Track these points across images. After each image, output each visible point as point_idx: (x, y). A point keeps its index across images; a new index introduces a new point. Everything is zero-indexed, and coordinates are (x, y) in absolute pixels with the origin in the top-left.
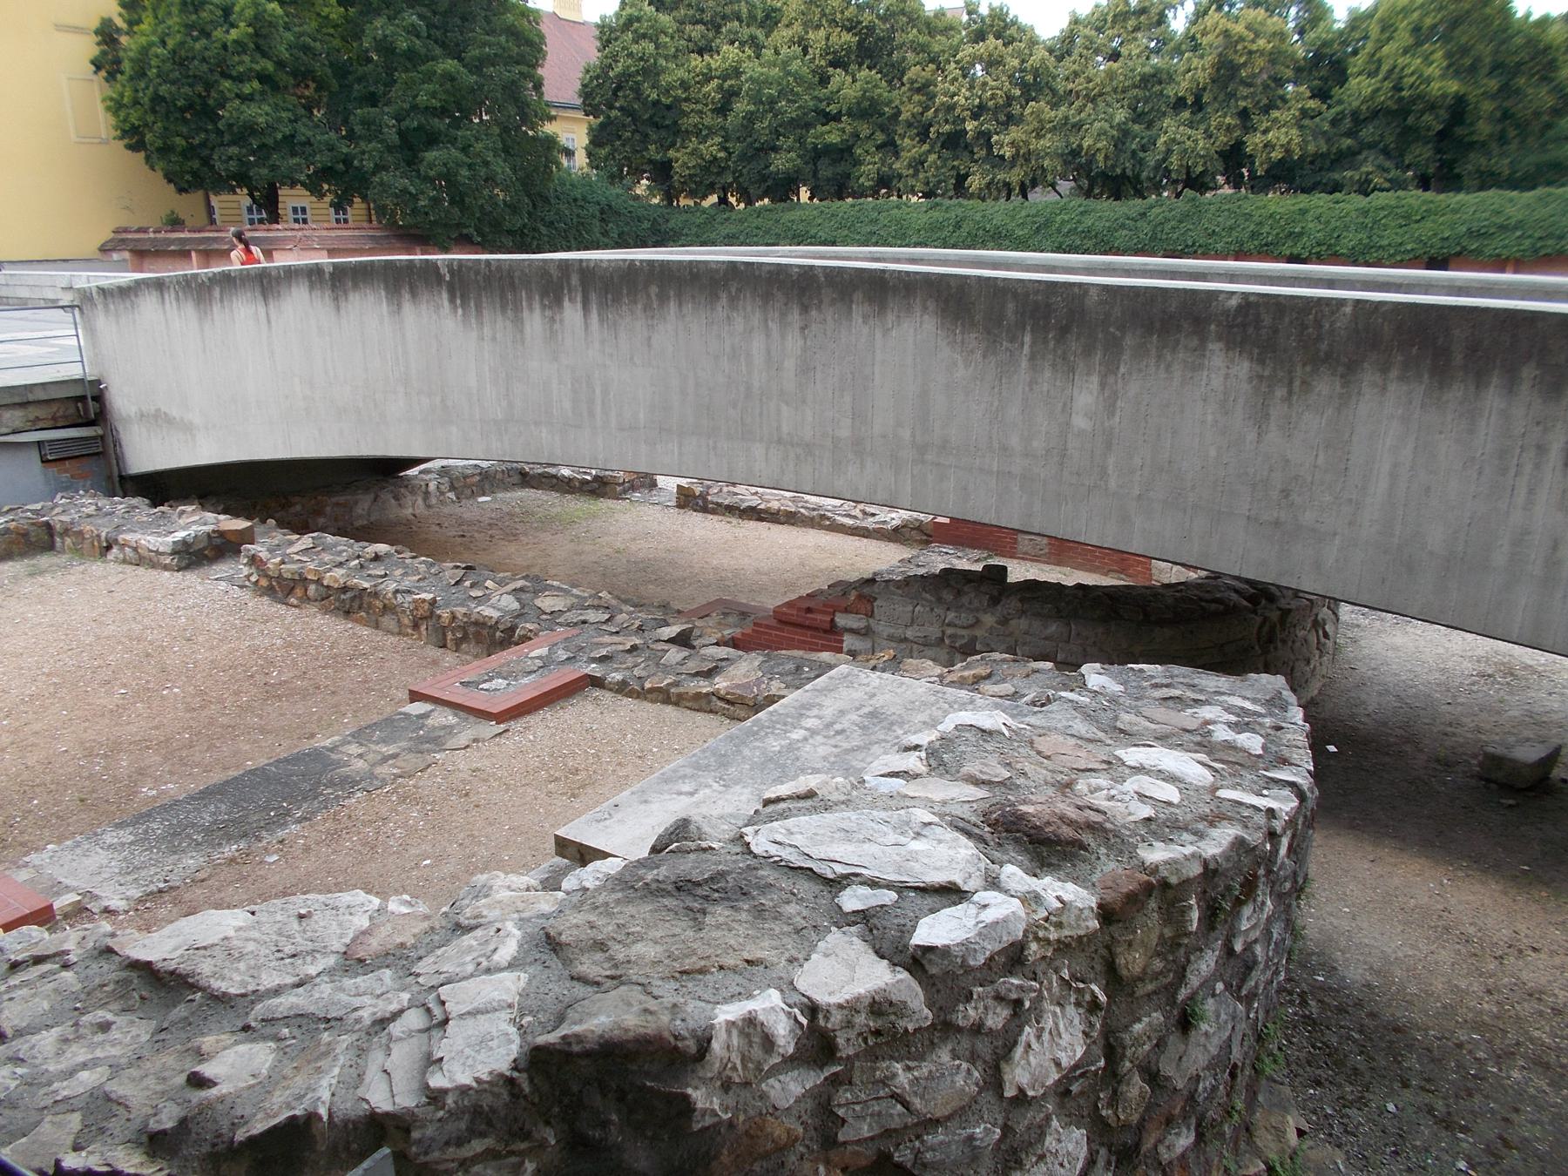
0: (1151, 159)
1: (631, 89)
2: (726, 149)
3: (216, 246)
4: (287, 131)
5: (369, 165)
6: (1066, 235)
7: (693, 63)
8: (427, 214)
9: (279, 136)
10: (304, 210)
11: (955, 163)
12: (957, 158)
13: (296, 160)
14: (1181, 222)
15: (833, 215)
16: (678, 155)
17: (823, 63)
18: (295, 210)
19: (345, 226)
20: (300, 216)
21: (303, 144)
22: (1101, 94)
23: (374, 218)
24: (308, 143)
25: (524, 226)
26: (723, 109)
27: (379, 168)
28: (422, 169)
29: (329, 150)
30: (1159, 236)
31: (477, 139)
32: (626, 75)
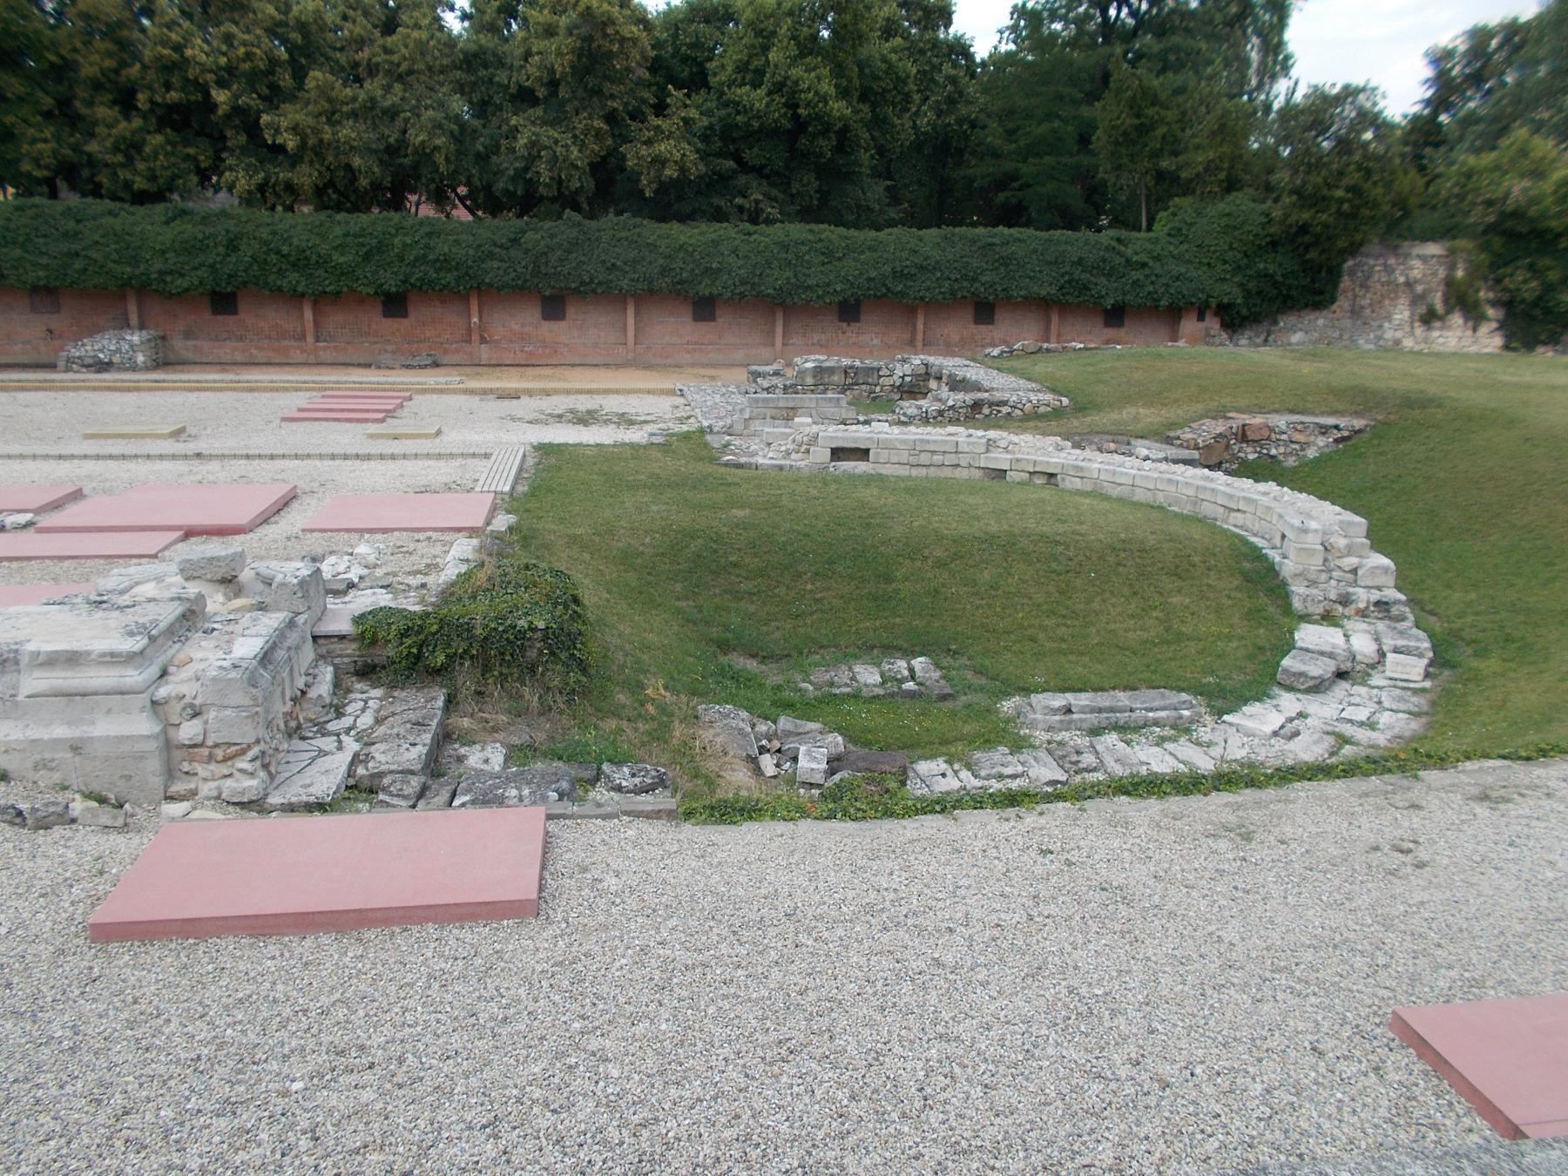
0: (507, 165)
6: (413, 264)
11: (191, 151)
22: (410, 72)
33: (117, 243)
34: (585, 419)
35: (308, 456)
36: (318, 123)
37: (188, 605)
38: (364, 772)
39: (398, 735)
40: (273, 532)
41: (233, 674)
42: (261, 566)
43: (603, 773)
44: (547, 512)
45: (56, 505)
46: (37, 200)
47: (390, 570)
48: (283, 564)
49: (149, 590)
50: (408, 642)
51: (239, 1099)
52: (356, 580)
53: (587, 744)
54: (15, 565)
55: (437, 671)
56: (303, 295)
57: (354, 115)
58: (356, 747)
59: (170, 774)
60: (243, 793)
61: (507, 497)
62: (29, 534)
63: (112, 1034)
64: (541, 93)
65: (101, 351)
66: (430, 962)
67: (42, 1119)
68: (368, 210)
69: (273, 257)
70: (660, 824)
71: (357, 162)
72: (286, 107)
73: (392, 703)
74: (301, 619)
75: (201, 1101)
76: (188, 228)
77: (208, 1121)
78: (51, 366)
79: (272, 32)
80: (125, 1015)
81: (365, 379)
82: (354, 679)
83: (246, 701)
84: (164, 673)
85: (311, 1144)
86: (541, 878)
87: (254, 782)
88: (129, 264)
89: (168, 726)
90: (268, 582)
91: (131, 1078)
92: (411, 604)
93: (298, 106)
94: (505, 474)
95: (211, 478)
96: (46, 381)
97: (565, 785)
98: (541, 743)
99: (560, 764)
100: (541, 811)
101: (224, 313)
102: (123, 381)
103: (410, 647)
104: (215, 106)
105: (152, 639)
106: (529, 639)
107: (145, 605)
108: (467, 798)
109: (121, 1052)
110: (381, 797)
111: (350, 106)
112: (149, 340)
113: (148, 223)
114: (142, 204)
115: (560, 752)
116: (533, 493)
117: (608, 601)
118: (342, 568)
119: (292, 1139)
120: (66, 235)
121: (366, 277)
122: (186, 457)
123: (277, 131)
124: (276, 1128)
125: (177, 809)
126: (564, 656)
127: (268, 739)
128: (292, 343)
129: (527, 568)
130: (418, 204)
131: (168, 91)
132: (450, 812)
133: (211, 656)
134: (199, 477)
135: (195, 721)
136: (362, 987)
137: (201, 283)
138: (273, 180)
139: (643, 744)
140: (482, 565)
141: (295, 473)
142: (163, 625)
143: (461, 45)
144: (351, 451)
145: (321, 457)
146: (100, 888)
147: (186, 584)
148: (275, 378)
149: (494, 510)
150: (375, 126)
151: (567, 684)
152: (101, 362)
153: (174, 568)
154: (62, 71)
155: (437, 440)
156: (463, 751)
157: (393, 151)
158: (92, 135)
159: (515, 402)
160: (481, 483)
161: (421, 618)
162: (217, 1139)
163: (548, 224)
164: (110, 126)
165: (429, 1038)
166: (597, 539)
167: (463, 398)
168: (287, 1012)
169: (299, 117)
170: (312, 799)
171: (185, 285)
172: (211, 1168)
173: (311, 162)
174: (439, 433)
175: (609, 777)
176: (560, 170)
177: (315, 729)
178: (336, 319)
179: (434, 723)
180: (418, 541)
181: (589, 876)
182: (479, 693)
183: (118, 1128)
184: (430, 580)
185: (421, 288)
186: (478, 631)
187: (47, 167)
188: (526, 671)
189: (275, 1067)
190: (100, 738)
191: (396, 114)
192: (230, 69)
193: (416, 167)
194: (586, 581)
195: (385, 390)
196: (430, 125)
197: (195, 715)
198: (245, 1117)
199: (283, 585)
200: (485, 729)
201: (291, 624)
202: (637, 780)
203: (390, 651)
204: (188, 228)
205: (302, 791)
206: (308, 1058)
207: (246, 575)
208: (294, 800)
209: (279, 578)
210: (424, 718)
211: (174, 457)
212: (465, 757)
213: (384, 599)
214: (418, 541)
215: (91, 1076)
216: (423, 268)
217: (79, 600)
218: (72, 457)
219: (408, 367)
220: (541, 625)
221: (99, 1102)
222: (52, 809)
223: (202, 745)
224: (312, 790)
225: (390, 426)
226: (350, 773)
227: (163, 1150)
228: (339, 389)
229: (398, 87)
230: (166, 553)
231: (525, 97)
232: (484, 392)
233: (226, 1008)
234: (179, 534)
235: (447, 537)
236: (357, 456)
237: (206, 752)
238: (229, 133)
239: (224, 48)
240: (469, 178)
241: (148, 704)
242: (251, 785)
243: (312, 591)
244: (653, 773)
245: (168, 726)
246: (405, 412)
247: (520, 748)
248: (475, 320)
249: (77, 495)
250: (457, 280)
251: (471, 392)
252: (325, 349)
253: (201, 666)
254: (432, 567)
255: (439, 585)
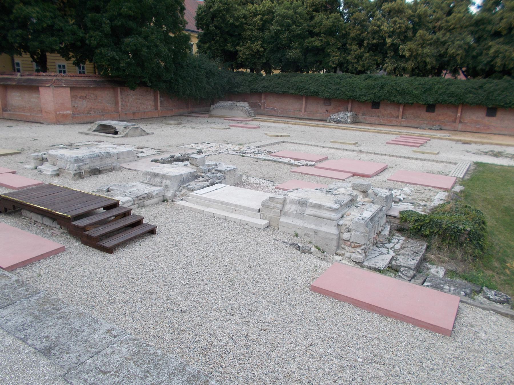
0: (484, 59)
1: (221, 17)
2: (262, 47)
3: (9, 83)
4: (50, 22)
5: (94, 43)
6: (440, 95)
7: (249, 7)
8: (124, 71)
9: (45, 25)
10: (64, 67)
11: (376, 58)
12: (375, 56)
13: (54, 38)
14: (503, 91)
15: (317, 80)
16: (242, 49)
17: (311, 10)
18: (60, 66)
19: (84, 75)
20: (62, 69)
21: (58, 30)
22: (454, 28)
23: (97, 71)
24: (61, 30)
25: (172, 78)
26: (262, 29)
27: (99, 46)
28: (123, 47)
29: (72, 35)
30: (491, 98)
31: (152, 33)
32: (219, 11)
33: (350, 86)
34: (497, 155)
35: (393, 156)
36: (418, 47)
37: (353, 197)
38: (395, 264)
39: (408, 254)
40: (378, 178)
41: (362, 222)
42: (375, 189)
43: (483, 290)
44: (476, 187)
45: (321, 161)
46: (331, 73)
47: (414, 198)
48: (382, 190)
49: (342, 190)
50: (417, 224)
51: (342, 356)
52: (402, 199)
53: (478, 278)
54: (308, 176)
55: (426, 236)
56: (401, 104)
57: (431, 44)
58: (393, 254)
59: (338, 247)
60: (357, 259)
61: (461, 180)
62: (313, 168)
63: (311, 319)
64: (504, 32)
65: (339, 117)
66: (409, 337)
67: (291, 337)
68: (428, 76)
69: (394, 91)
70: (507, 319)
71: (428, 60)
72: (409, 43)
73: (407, 243)
74: (384, 208)
75: (332, 351)
76: (370, 82)
77: (333, 359)
78: (325, 121)
79: (409, 19)
80: (316, 315)
81: (415, 132)
82: (396, 231)
83: (364, 231)
84: (342, 217)
85: (361, 381)
86: (454, 323)
87: (361, 257)
88: (351, 92)
89: (341, 232)
90: (376, 195)
91: (314, 335)
92: (420, 211)
93: (412, 42)
94: (461, 171)
95: (363, 159)
96: (324, 125)
97: (468, 291)
98: (460, 272)
99: (466, 282)
100: (458, 298)
101: (374, 108)
102: (343, 127)
103: (418, 226)
104: (387, 44)
105: (341, 206)
106: (462, 233)
107: (341, 195)
108: (429, 284)
109: (313, 326)
110: (400, 274)
111: (430, 42)
112: (352, 115)
113: (359, 80)
114: (359, 74)
115: (466, 277)
116: (471, 180)
117: (496, 225)
118: (398, 194)
119: (356, 377)
120: (337, 83)
121: (423, 98)
122: (357, 151)
123: (404, 51)
124: (352, 371)
125: (339, 258)
126: (475, 242)
127: (368, 244)
128: (394, 119)
129: (466, 207)
130: (445, 74)
131: (373, 40)
132: (423, 287)
133: (356, 215)
134: (359, 158)
135: (348, 233)
136: (385, 336)
137: (370, 99)
138: (399, 67)
139: (502, 284)
140: (449, 203)
141: (387, 161)
142: (345, 202)
143: (475, 18)
144: (407, 156)
145: (397, 156)
146: (315, 275)
147: (353, 191)
148: (387, 129)
149: (455, 183)
150: (437, 48)
151: (474, 253)
152: (338, 121)
153: (350, 185)
154: (345, 36)
155: (437, 156)
156: (430, 266)
157: (441, 56)
158: (350, 54)
159: (469, 145)
160: (452, 173)
161: (424, 217)
162: (334, 365)
163: (496, 81)
164: (355, 51)
165: (404, 363)
166: (495, 201)
167: (449, 142)
168: (360, 334)
169: (412, 46)
170: (377, 267)
171: (366, 99)
172: (331, 374)
173: (413, 61)
174: (438, 153)
175: (485, 292)
176: (506, 61)
177: (381, 245)
178: (410, 112)
179: (421, 254)
180: (425, 189)
181: (474, 329)
182: (439, 248)
183: (309, 349)
184: (428, 204)
185: (441, 103)
186: (444, 226)
187: (336, 64)
188: (459, 244)
189: (354, 351)
190: (322, 231)
191: (446, 43)
192: (393, 32)
193: (449, 61)
194: (488, 216)
195: (421, 136)
196: (457, 46)
197: (349, 231)
198: (343, 362)
199: (381, 196)
200: (439, 261)
201: (381, 210)
202: (497, 298)
203: (410, 225)
204: (370, 82)
205: (374, 264)
206: (364, 352)
207: (370, 191)
208: (371, 266)
209: (380, 194)
210: (418, 251)
211: (354, 151)
212: (430, 268)
213: (411, 207)
214: (425, 189)
215: (304, 330)
216: (443, 96)
217: (324, 190)
218: (327, 147)
219: (431, 129)
220: (468, 229)
221: (305, 338)
222: (307, 248)
223: (349, 241)
224: (377, 264)
225: (421, 149)
226: (390, 262)
227: (319, 361)
228: (406, 135)
229: (448, 34)
230: (347, 180)
231: (497, 34)
232: (457, 141)
233: (343, 325)
234: (352, 174)
235: (436, 190)
236: (409, 158)
237: (349, 243)
238: (388, 52)
239: (393, 25)
240: (468, 65)
241: (337, 225)
242: (360, 257)
243: (389, 200)
244: (505, 297)
245: (341, 232)
246: (427, 145)
247: (452, 271)
248: (459, 115)
249: (326, 159)
250: (455, 101)
251: (451, 140)
252: (404, 121)
253: (353, 217)
254: (428, 200)
255: (431, 206)
